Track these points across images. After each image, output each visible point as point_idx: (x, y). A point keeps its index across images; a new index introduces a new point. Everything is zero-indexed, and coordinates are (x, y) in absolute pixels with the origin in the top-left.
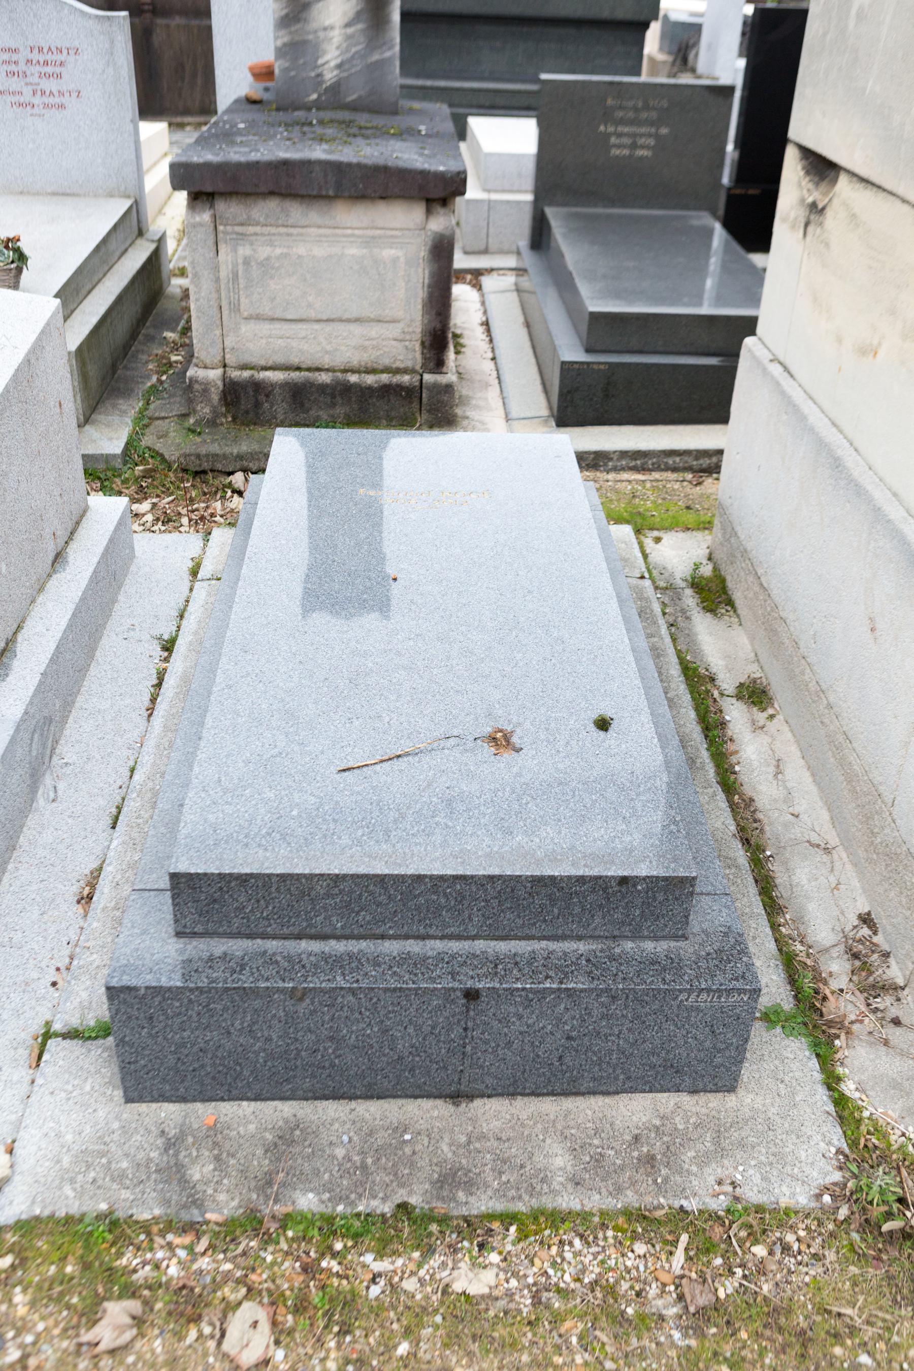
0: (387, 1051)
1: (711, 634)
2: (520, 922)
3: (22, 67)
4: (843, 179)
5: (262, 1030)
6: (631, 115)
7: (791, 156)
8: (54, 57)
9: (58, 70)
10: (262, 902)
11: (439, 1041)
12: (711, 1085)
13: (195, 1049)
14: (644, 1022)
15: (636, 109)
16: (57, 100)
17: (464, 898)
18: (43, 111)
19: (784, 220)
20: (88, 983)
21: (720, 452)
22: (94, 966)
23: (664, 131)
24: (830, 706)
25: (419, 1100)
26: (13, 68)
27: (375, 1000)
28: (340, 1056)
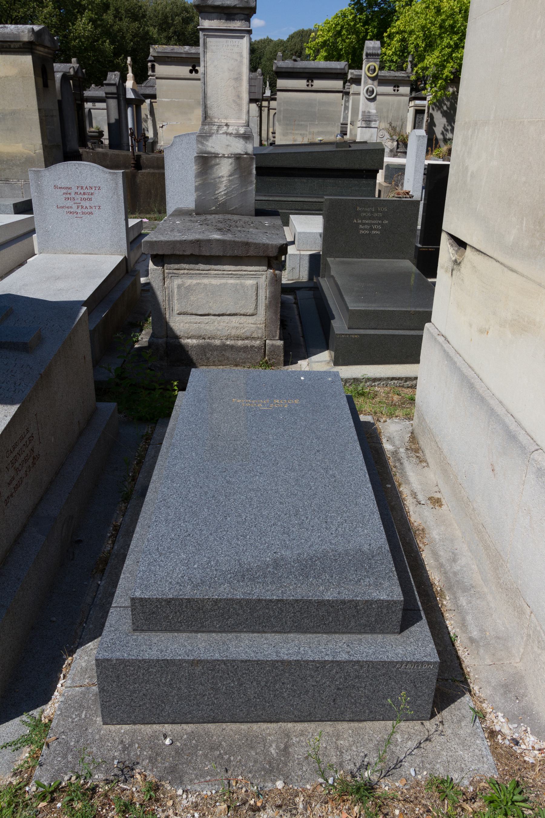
0: (242, 695)
1: (414, 472)
2: (312, 624)
3: (73, 195)
4: (468, 248)
5: (176, 683)
6: (369, 214)
7: (444, 238)
8: (88, 191)
9: (90, 197)
10: (178, 613)
11: (269, 690)
12: (415, 716)
13: (141, 694)
14: (378, 680)
15: (372, 212)
16: (89, 210)
17: (282, 611)
18: (82, 216)
19: (442, 268)
20: (86, 658)
21: (416, 378)
22: (89, 649)
23: (386, 222)
24: (474, 509)
25: (259, 723)
26: (68, 196)
27: (236, 667)
28: (217, 698)
